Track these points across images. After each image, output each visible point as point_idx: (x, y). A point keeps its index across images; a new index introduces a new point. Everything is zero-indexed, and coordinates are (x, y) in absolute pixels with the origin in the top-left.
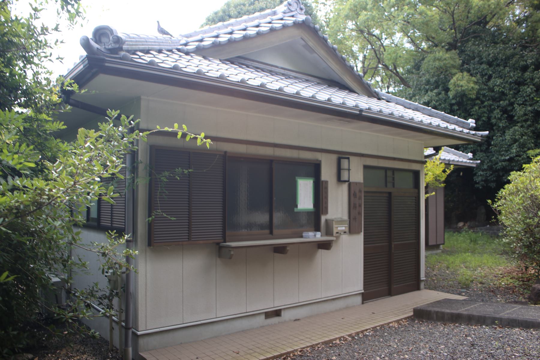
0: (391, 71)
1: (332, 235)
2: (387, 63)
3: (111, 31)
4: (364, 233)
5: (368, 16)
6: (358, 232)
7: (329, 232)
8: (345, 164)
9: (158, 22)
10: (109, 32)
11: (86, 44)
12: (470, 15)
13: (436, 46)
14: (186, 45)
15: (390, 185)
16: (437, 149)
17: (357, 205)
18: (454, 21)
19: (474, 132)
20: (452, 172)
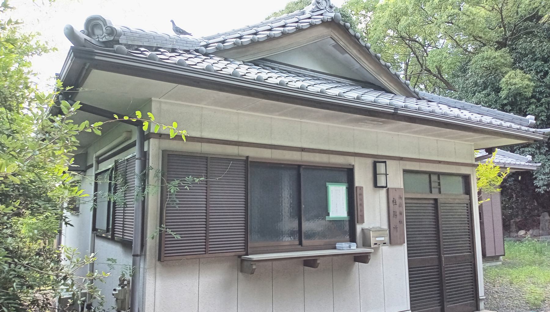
0: (434, 76)
1: (369, 246)
2: (430, 68)
3: (104, 21)
4: (408, 244)
5: (409, 21)
6: (401, 244)
7: (366, 243)
8: (381, 168)
9: (172, 21)
10: (102, 23)
11: (71, 34)
12: (519, 9)
13: (485, 45)
14: (206, 46)
15: (435, 191)
16: (490, 151)
17: (398, 213)
18: (502, 18)
19: (534, 130)
20: (509, 176)
